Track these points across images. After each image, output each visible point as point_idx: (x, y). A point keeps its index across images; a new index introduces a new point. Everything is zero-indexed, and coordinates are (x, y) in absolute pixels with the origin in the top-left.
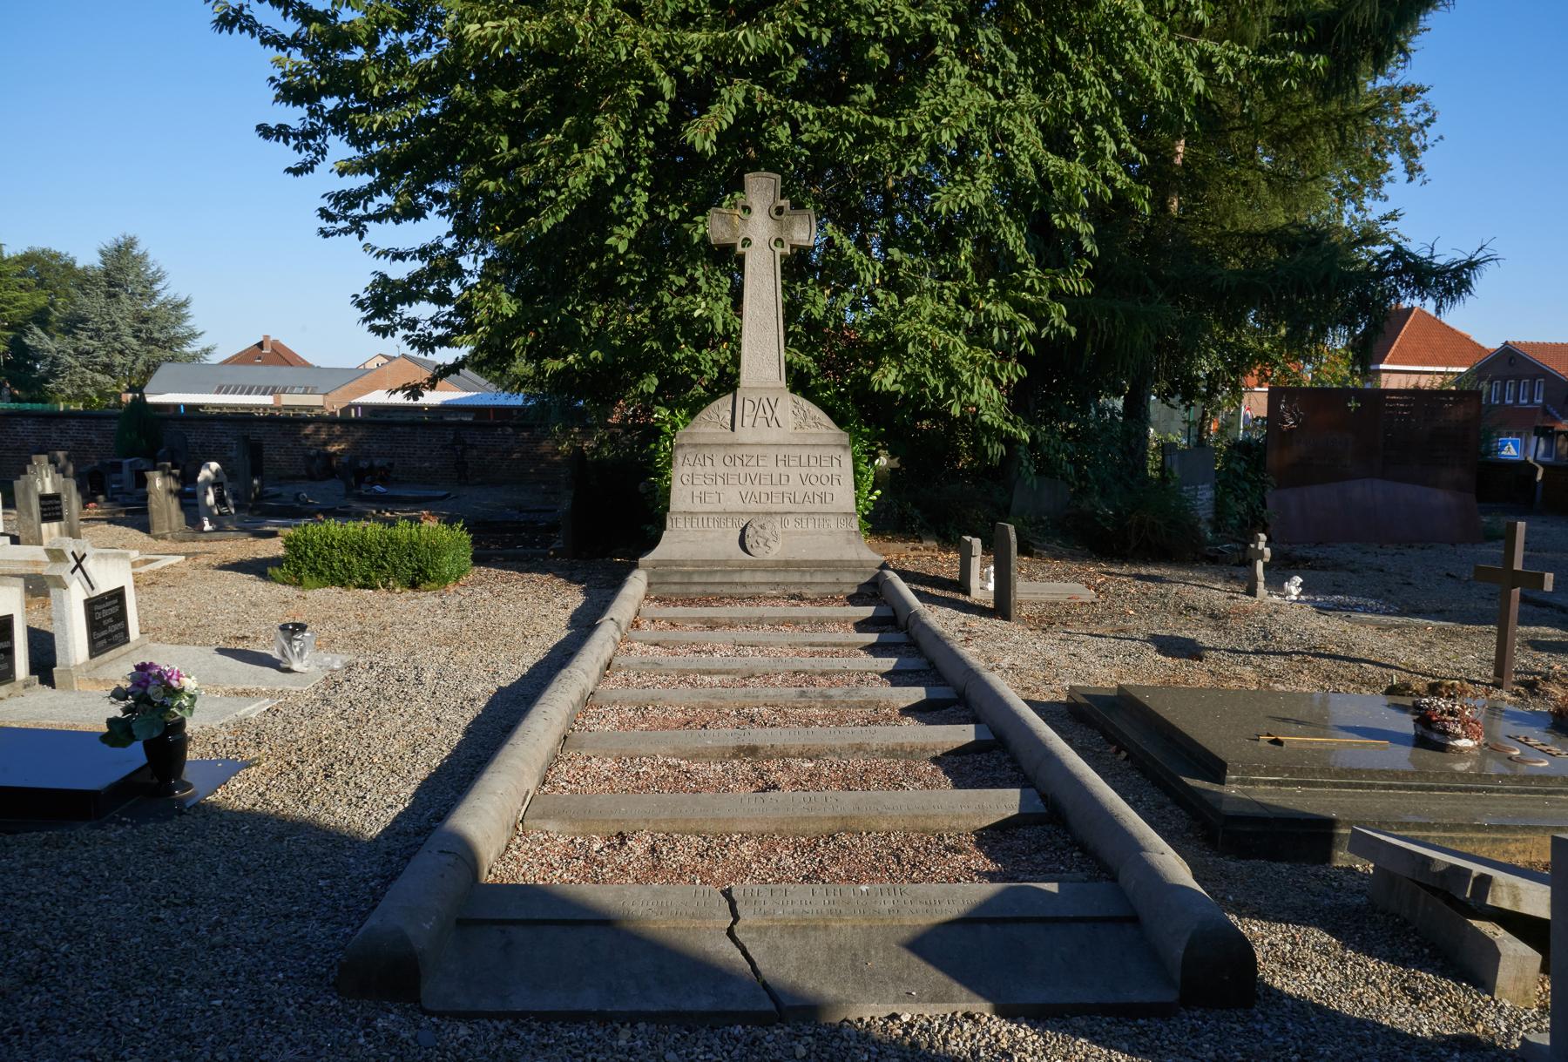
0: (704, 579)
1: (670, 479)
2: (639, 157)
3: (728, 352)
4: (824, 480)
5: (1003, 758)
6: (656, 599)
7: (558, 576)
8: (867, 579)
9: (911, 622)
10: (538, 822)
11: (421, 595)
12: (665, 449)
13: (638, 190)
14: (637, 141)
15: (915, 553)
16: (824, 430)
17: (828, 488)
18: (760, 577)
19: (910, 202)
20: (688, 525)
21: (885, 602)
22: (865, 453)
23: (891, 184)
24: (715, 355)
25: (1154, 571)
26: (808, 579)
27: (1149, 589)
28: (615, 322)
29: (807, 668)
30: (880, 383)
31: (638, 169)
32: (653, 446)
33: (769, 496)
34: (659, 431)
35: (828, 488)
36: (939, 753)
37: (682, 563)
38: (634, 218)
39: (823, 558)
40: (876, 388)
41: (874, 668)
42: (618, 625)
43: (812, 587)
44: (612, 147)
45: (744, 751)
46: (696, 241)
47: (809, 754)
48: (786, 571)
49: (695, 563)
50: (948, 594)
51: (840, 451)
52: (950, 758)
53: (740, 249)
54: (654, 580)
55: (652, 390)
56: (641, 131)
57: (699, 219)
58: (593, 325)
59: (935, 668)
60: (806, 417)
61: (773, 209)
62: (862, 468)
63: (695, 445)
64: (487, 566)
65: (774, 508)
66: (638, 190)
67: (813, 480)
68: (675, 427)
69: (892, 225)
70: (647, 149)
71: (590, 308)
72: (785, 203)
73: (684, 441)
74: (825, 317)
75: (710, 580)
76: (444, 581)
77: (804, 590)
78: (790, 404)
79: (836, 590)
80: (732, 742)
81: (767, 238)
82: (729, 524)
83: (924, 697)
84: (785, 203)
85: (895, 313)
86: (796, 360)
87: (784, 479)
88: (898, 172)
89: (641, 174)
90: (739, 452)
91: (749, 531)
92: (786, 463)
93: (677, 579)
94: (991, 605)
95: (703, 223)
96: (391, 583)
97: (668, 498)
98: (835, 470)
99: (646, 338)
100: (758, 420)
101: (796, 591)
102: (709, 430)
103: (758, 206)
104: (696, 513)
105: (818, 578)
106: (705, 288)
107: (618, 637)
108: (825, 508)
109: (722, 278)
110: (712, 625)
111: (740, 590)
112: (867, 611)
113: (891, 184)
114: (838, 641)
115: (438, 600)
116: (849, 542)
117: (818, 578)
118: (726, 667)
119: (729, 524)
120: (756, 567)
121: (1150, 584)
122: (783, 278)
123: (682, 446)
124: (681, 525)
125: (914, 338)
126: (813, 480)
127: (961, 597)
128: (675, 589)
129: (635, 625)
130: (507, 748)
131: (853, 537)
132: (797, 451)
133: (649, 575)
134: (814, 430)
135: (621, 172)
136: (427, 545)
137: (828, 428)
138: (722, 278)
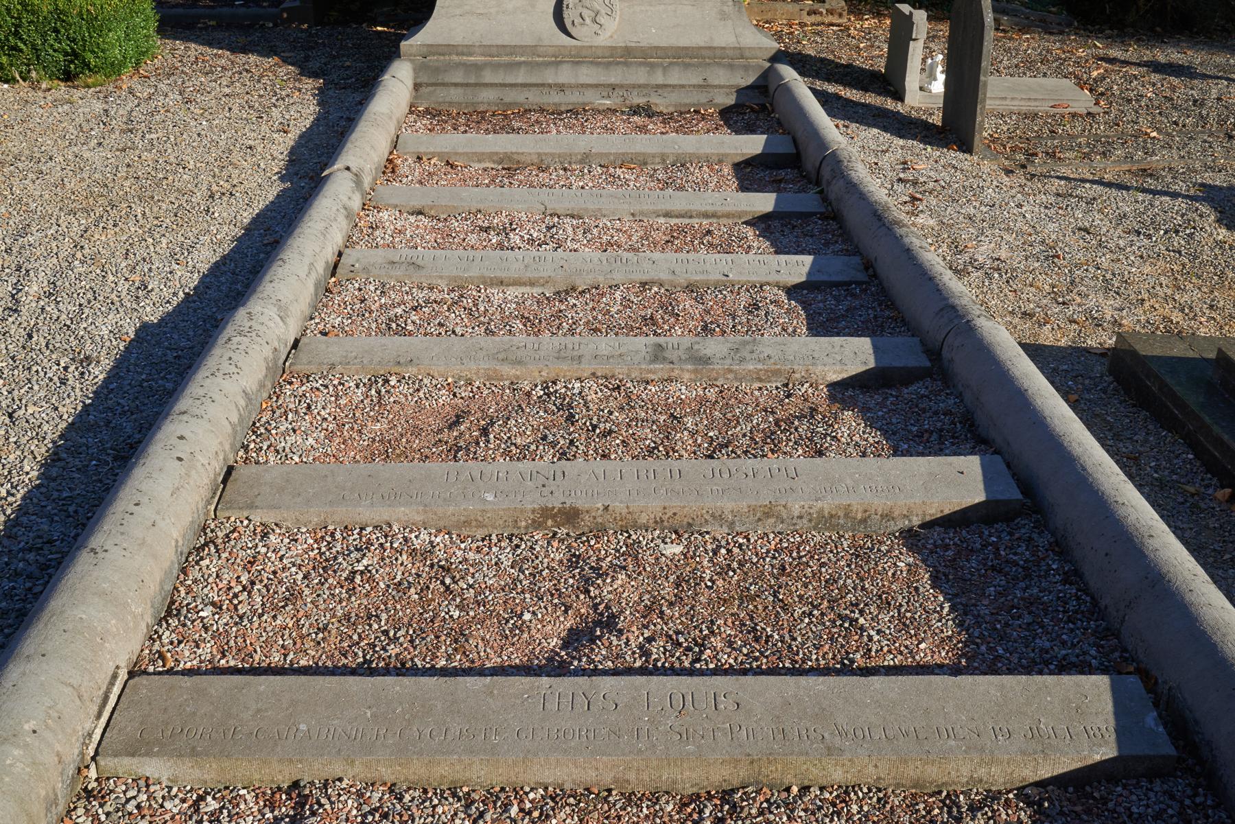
0: (498, 78)
5: (1042, 541)
6: (427, 111)
7: (286, 61)
8: (750, 80)
9: (826, 173)
10: (127, 761)
11: (77, 94)
15: (813, 19)
18: (587, 75)
21: (779, 123)
25: (1174, 55)
26: (659, 78)
27: (1173, 89)
29: (664, 276)
36: (916, 521)
37: (467, 50)
41: (773, 278)
45: (553, 517)
46: (1230, 490)
47: (676, 522)
48: (626, 64)
49: (487, 50)
50: (871, 99)
52: (937, 532)
54: (424, 79)
59: (875, 276)
64: (186, 39)
76: (113, 69)
79: (703, 98)
80: (532, 502)
83: (872, 364)
93: (458, 77)
94: (937, 119)
96: (34, 74)
101: (641, 101)
105: (675, 77)
107: (356, 203)
110: (510, 167)
111: (554, 98)
112: (754, 144)
114: (710, 209)
115: (98, 107)
116: (724, 16)
117: (675, 77)
118: (529, 275)
120: (579, 58)
121: (1175, 81)
127: (890, 104)
128: (455, 95)
129: (390, 168)
130: (83, 562)
133: (417, 71)
136: (80, 15)
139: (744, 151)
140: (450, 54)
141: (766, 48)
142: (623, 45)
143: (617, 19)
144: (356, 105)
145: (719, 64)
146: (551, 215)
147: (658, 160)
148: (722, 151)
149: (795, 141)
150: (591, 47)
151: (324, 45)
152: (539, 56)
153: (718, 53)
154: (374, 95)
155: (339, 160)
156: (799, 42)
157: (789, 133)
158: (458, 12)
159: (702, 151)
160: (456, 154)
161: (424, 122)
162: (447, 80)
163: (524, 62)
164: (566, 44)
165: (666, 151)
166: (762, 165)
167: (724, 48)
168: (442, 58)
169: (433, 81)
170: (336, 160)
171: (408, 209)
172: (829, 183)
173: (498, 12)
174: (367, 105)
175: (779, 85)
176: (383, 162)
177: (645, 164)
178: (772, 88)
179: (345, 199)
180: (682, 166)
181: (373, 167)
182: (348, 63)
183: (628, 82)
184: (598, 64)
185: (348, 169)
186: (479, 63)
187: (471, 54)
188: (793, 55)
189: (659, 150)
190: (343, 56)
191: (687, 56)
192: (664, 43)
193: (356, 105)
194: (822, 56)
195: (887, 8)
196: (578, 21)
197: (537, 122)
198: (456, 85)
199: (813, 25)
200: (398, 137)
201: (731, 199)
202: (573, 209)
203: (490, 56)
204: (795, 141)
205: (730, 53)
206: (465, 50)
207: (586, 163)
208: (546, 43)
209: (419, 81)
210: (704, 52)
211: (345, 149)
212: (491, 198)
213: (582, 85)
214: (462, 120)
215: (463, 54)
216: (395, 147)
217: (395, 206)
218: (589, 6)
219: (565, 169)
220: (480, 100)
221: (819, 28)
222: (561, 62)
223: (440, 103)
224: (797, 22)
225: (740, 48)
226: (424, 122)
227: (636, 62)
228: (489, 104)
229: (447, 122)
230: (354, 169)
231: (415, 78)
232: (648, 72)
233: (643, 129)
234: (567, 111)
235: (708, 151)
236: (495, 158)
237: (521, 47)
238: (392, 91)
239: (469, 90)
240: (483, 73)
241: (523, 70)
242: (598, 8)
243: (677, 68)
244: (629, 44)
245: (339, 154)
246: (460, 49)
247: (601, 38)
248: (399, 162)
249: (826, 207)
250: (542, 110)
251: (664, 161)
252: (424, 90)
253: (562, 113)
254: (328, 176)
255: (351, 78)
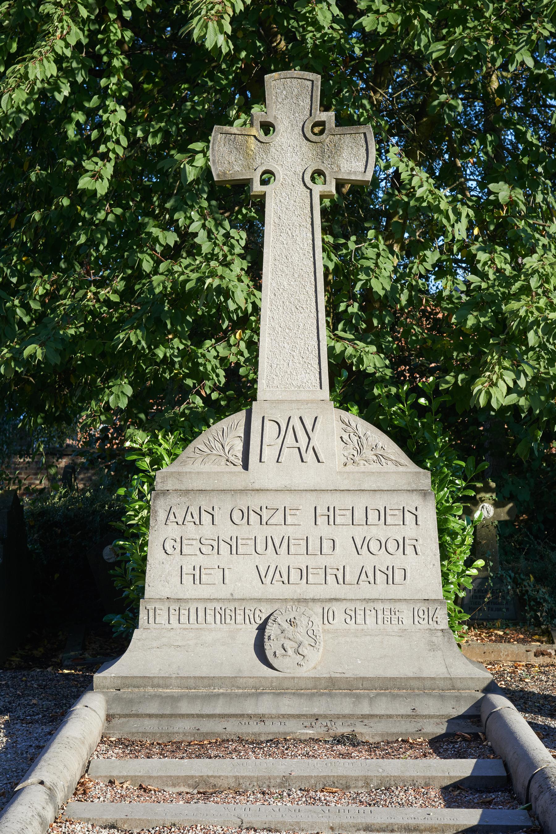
0: (195, 710)
1: (146, 544)
2: (111, 56)
3: (243, 345)
4: (392, 546)
8: (462, 710)
9: (534, 790)
12: (142, 495)
13: (111, 104)
14: (106, 31)
15: (541, 660)
16: (391, 467)
17: (398, 560)
19: (524, 110)
20: (174, 619)
21: (492, 750)
22: (457, 500)
23: (495, 84)
24: (222, 349)
26: (365, 709)
28: (68, 302)
30: (489, 396)
31: (109, 71)
32: (122, 491)
33: (304, 573)
34: (133, 468)
35: (398, 560)
38: (111, 145)
39: (391, 673)
40: (482, 401)
42: (51, 792)
43: (372, 722)
44: (67, 45)
48: (330, 695)
51: (415, 501)
53: (257, 188)
54: (117, 710)
55: (123, 403)
56: (113, 16)
57: (198, 146)
58: (35, 306)
60: (361, 446)
61: (309, 125)
62: (455, 524)
63: (187, 492)
65: (312, 592)
66: (111, 104)
67: (374, 546)
68: (157, 462)
69: (499, 146)
70: (121, 43)
71: (30, 280)
72: (329, 117)
73: (169, 486)
74: (394, 288)
75: (207, 710)
77: (360, 729)
78: (337, 426)
81: (300, 170)
82: (240, 618)
84: (329, 117)
85: (507, 281)
86: (350, 350)
87: (327, 545)
88: (504, 67)
89: (114, 80)
90: (255, 502)
91: (271, 630)
92: (331, 520)
93: (153, 708)
95: (204, 152)
97: (144, 572)
98: (410, 530)
99: (118, 327)
100: (285, 451)
102: (207, 467)
103: (286, 122)
104: (186, 600)
106: (206, 248)
107: (50, 815)
108: (393, 592)
109: (233, 232)
113: (495, 84)
116: (433, 647)
119: (240, 618)
122: (324, 230)
123: (165, 493)
124: (162, 619)
125: (536, 323)
126: (374, 546)
128: (150, 725)
131: (438, 639)
132: (348, 501)
134: (375, 467)
135: (80, 79)
137: (397, 463)
138: (233, 232)
139: (452, 774)
140: (145, 686)
141: (478, 679)
142: (327, 676)
143: (321, 651)
144: (45, 735)
145: (429, 695)
146: (247, 829)
147: (360, 783)
148: (428, 774)
149: (506, 765)
150: (293, 678)
151: (7, 685)
152: (239, 688)
153: (428, 684)
154: (66, 722)
155: (33, 774)
156: (521, 680)
157: (501, 758)
158: (155, 644)
159: (408, 774)
160: (150, 777)
161: (116, 751)
162: (141, 711)
163: (223, 694)
164: (267, 676)
165: (370, 774)
166: (471, 789)
167: (433, 679)
168: (137, 690)
169: (126, 712)
170: (30, 775)
171: (100, 823)
172: (537, 799)
173: (196, 644)
174: (60, 731)
175: (492, 713)
176: (75, 785)
177: (348, 787)
178: (484, 718)
179: (40, 808)
180: (387, 789)
181: (66, 785)
182: (34, 701)
183: (332, 712)
184: (301, 695)
185: (42, 783)
186: (176, 695)
187: (167, 687)
188: (514, 692)
189: (362, 774)
190: (29, 695)
191: (394, 687)
192: (370, 673)
193: (45, 735)
194: (547, 693)
195: (72, 325)
196: (280, 652)
197: (235, 750)
198: (150, 716)
199: (540, 666)
200: (89, 762)
201: (434, 813)
202: (270, 822)
203: (187, 688)
204: (506, 765)
205: (441, 684)
206: (161, 682)
207: (285, 787)
208: (246, 674)
209: (111, 712)
210: (413, 683)
211: (39, 766)
212: (186, 812)
213: (283, 716)
214: (156, 750)
215: (159, 686)
216: (87, 771)
217: (88, 821)
218: (291, 637)
219: (264, 793)
220: (175, 730)
221: (547, 669)
222: (261, 694)
223: (133, 734)
224: (524, 664)
225: (451, 679)
226: (116, 751)
227: (341, 693)
228: (185, 734)
229: (140, 751)
230: (47, 783)
231: (108, 709)
232: (354, 703)
233: (347, 755)
234: (268, 741)
235: (414, 774)
236: (190, 782)
237: (220, 678)
238: (84, 719)
239: (164, 721)
240: (179, 705)
241: (221, 701)
242: (301, 639)
243: (384, 699)
244: (333, 676)
245: (33, 770)
246: (156, 681)
247: (304, 668)
248: (91, 785)
249: (533, 822)
250: (240, 740)
251: (367, 784)
252: (115, 721)
253: (262, 742)
254: (23, 789)
255: (38, 714)
